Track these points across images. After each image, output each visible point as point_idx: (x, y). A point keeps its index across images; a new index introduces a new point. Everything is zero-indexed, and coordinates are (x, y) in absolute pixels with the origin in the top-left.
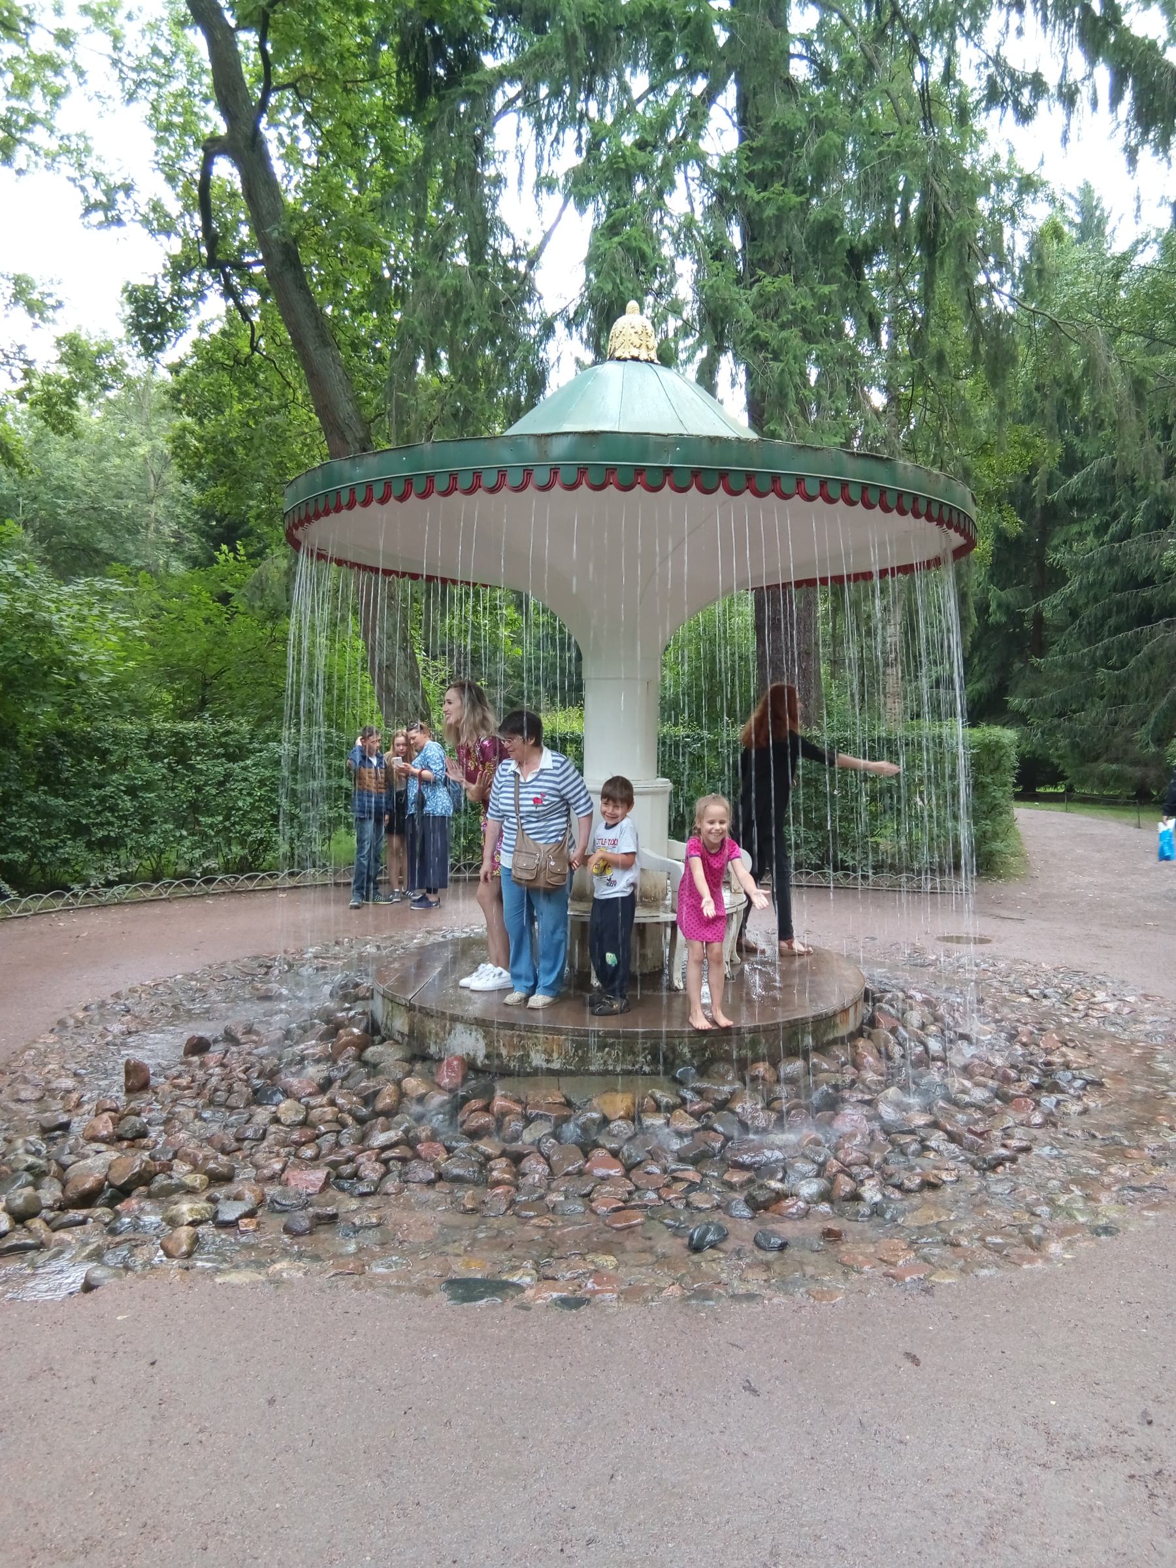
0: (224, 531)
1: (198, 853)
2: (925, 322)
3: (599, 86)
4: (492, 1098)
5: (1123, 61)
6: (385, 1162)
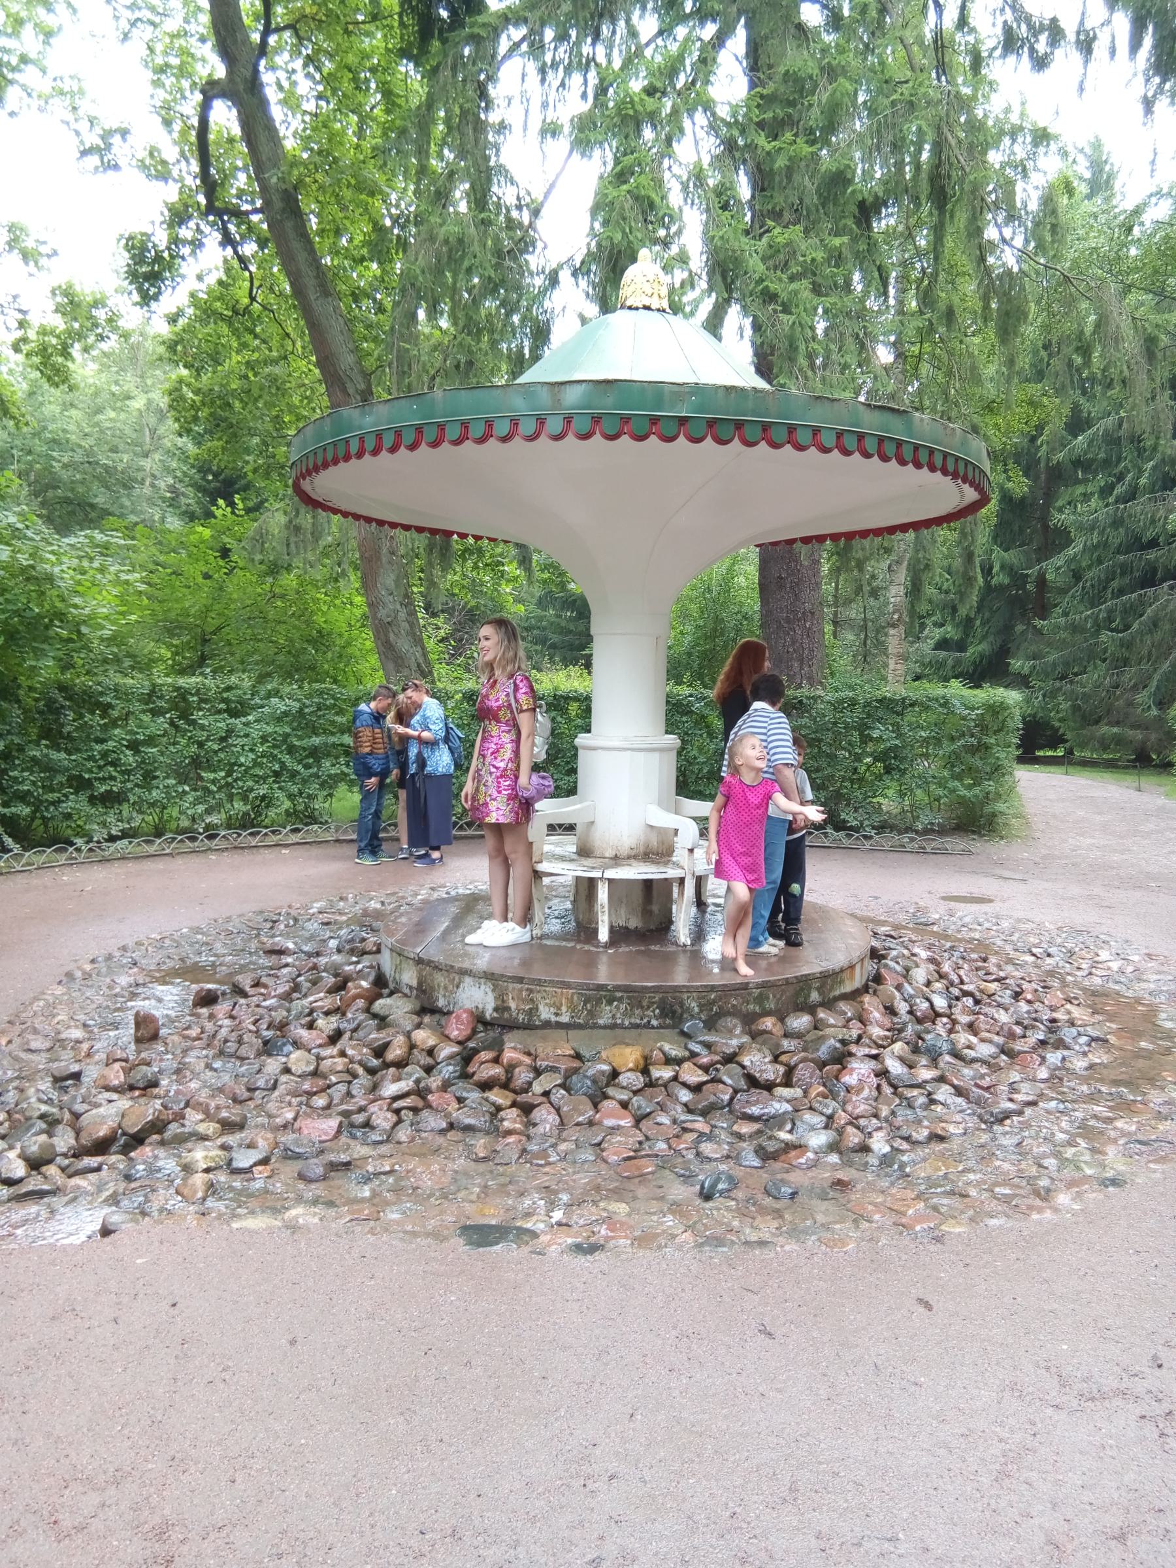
0: (220, 485)
1: (200, 808)
2: (935, 275)
3: (605, 30)
4: (501, 1051)
5: (1143, 6)
6: (397, 1112)
